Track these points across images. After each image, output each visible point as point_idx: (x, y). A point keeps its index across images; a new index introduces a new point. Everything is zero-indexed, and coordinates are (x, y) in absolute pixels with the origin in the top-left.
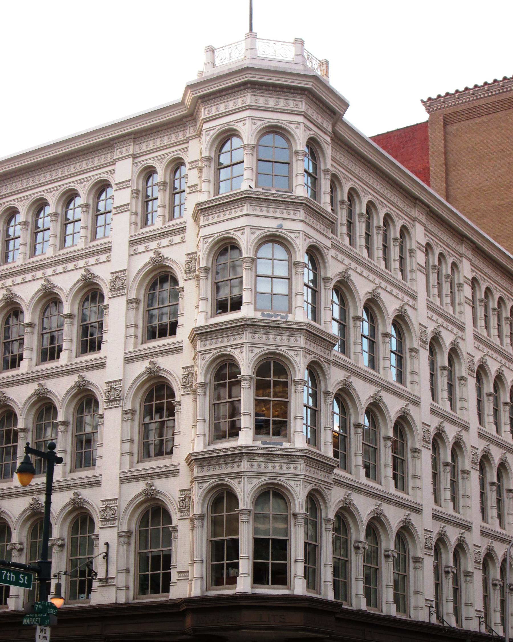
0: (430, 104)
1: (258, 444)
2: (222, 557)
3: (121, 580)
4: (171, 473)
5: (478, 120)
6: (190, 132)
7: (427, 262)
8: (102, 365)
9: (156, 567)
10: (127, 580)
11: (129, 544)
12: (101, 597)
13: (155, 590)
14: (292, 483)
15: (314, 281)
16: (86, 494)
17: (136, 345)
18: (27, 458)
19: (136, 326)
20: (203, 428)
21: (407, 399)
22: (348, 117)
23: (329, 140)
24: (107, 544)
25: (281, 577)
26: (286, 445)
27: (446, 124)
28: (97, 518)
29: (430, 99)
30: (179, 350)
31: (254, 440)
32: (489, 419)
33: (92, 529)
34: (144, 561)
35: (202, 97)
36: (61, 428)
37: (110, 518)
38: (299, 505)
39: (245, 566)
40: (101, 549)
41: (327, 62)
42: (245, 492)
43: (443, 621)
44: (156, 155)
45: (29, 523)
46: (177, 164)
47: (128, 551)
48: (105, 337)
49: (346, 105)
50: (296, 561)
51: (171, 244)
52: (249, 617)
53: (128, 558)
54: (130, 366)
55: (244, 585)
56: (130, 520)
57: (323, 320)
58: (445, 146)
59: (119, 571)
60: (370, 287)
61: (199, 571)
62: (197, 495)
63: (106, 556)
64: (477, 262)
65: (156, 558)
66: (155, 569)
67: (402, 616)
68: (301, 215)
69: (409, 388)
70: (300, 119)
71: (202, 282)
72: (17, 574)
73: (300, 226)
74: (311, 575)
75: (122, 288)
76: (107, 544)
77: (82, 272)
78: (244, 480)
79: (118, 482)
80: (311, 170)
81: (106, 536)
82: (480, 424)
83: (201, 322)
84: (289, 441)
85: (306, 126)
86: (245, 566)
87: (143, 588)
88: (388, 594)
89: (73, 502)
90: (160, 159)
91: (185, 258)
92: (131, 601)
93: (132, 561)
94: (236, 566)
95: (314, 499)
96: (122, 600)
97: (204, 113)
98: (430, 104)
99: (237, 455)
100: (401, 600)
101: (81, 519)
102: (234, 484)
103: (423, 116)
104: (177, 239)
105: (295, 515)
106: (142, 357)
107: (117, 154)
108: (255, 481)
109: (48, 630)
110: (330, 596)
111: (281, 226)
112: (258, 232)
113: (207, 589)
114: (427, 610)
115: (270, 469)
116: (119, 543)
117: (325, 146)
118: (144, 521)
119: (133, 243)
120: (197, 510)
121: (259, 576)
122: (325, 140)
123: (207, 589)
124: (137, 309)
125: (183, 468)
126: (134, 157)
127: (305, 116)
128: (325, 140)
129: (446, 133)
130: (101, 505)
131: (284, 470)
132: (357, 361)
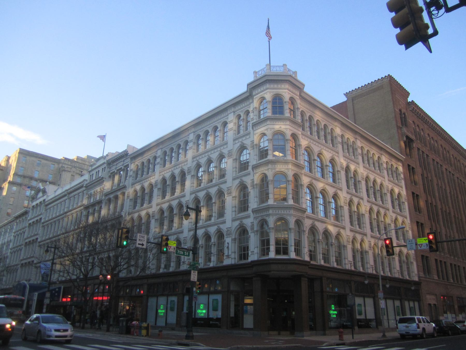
0: (346, 95)
1: (275, 203)
2: (265, 244)
3: (233, 256)
4: (248, 217)
5: (364, 97)
6: (251, 101)
7: (342, 141)
8: (226, 182)
9: (244, 251)
10: (235, 256)
11: (235, 243)
12: (227, 262)
13: (245, 259)
14: (288, 217)
15: (295, 146)
16: (221, 226)
17: (236, 174)
18: (187, 210)
19: (236, 168)
20: (257, 200)
21: (337, 188)
22: (306, 90)
23: (298, 98)
24: (228, 243)
25: (286, 252)
26: (286, 203)
27: (353, 100)
28: (225, 234)
29: (347, 93)
30: (249, 174)
31: (274, 202)
32: (372, 196)
33: (224, 239)
34: (240, 248)
35: (252, 88)
36: (214, 204)
37: (229, 234)
38: (292, 225)
39: (272, 248)
40: (226, 245)
41: (296, 72)
42: (271, 221)
43: (404, 277)
44: (240, 110)
45: (205, 238)
46: (248, 113)
47: (235, 246)
48: (226, 173)
49: (304, 85)
50: (291, 246)
51: (246, 139)
52: (274, 267)
53: (235, 247)
54: (234, 181)
55: (272, 255)
56: (235, 235)
57: (299, 159)
58: (353, 108)
59: (232, 252)
60: (319, 149)
61: (257, 251)
62: (256, 222)
63: (228, 247)
64: (362, 141)
65: (244, 248)
66: (244, 251)
67: (339, 267)
68: (288, 123)
69: (358, 194)
70: (286, 91)
71: (255, 149)
72: (184, 252)
73: (288, 127)
74: (298, 251)
75: (231, 156)
76: (228, 243)
77: (219, 152)
78: (271, 217)
79: (231, 222)
80: (292, 108)
81: (228, 240)
82: (368, 197)
83: (255, 163)
84: (287, 202)
85: (289, 93)
86: (272, 248)
87: (240, 258)
88: (387, 269)
89: (217, 229)
90: (242, 111)
91: (250, 143)
92: (236, 263)
93: (236, 249)
94: (269, 248)
95: (298, 223)
96: (233, 263)
97: (254, 93)
98: (346, 95)
99: (268, 208)
100: (339, 261)
101: (220, 235)
102: (267, 218)
103: (345, 99)
104: (248, 137)
105: (290, 229)
106: (238, 178)
107: (229, 112)
108: (275, 217)
109: (196, 272)
110: (307, 258)
111: (281, 127)
112: (272, 130)
113: (260, 257)
114: (371, 269)
115: (280, 212)
116: (232, 242)
117: (297, 100)
118: (240, 235)
119: (234, 140)
120: (255, 229)
121: (278, 252)
122: (297, 98)
123: (260, 257)
124: (236, 162)
125: (252, 214)
126: (234, 112)
127: (288, 90)
128: (297, 98)
129: (353, 104)
130: (226, 230)
131: (285, 213)
132: (315, 175)
